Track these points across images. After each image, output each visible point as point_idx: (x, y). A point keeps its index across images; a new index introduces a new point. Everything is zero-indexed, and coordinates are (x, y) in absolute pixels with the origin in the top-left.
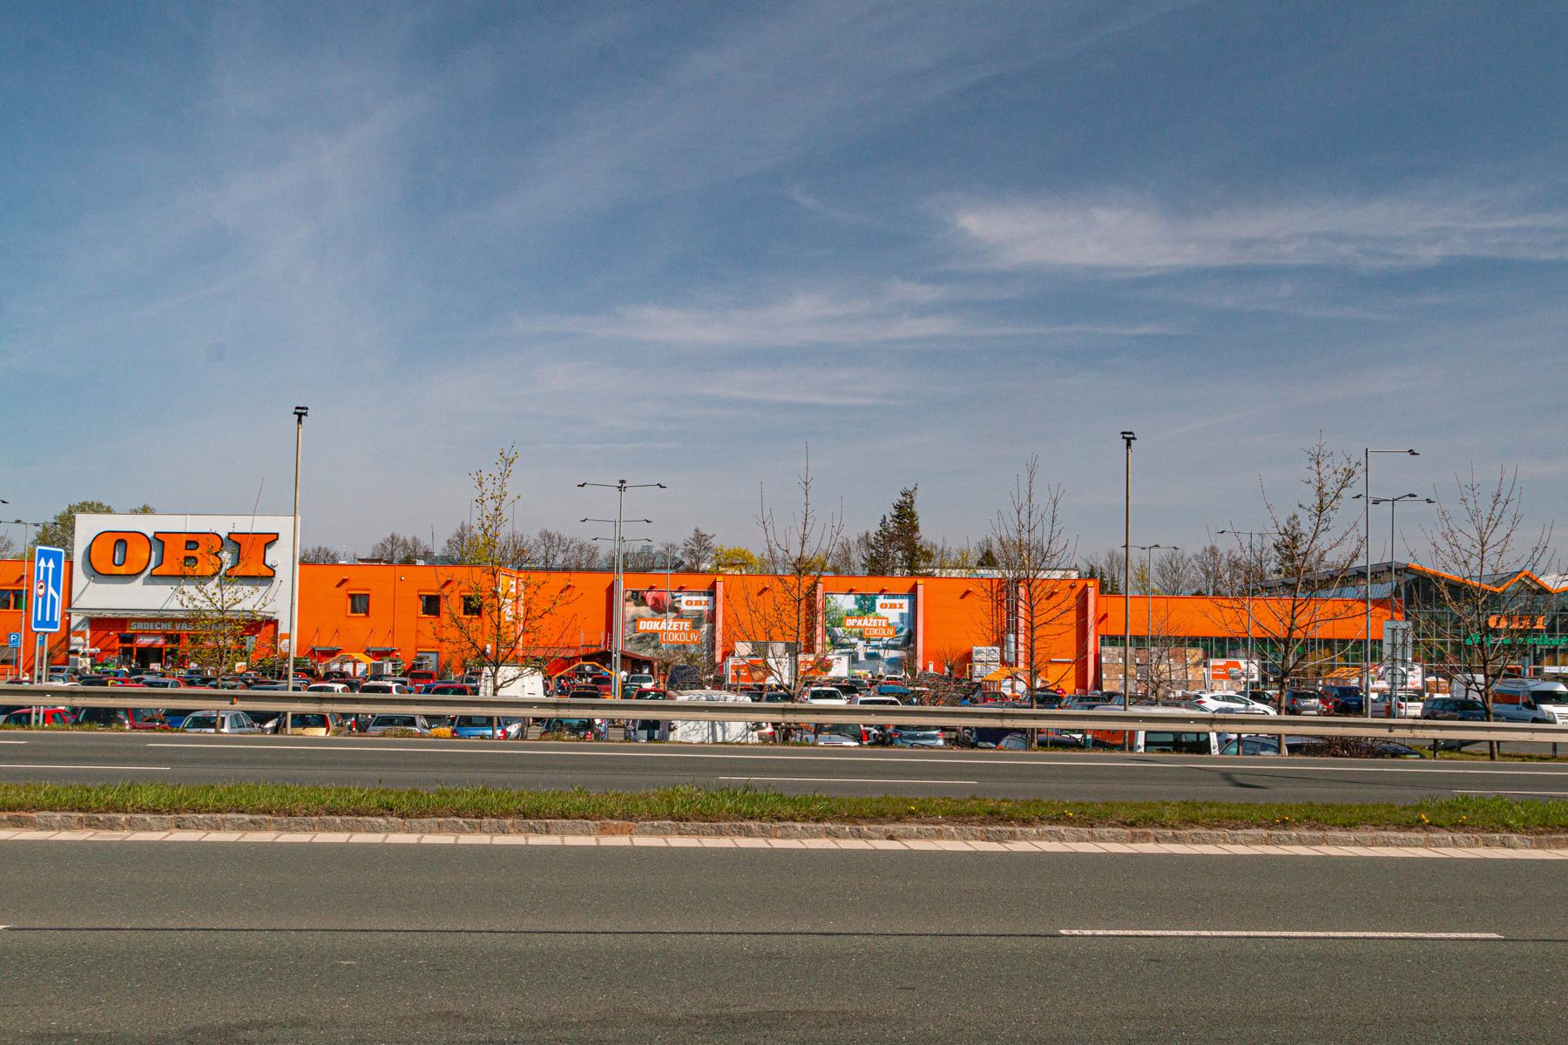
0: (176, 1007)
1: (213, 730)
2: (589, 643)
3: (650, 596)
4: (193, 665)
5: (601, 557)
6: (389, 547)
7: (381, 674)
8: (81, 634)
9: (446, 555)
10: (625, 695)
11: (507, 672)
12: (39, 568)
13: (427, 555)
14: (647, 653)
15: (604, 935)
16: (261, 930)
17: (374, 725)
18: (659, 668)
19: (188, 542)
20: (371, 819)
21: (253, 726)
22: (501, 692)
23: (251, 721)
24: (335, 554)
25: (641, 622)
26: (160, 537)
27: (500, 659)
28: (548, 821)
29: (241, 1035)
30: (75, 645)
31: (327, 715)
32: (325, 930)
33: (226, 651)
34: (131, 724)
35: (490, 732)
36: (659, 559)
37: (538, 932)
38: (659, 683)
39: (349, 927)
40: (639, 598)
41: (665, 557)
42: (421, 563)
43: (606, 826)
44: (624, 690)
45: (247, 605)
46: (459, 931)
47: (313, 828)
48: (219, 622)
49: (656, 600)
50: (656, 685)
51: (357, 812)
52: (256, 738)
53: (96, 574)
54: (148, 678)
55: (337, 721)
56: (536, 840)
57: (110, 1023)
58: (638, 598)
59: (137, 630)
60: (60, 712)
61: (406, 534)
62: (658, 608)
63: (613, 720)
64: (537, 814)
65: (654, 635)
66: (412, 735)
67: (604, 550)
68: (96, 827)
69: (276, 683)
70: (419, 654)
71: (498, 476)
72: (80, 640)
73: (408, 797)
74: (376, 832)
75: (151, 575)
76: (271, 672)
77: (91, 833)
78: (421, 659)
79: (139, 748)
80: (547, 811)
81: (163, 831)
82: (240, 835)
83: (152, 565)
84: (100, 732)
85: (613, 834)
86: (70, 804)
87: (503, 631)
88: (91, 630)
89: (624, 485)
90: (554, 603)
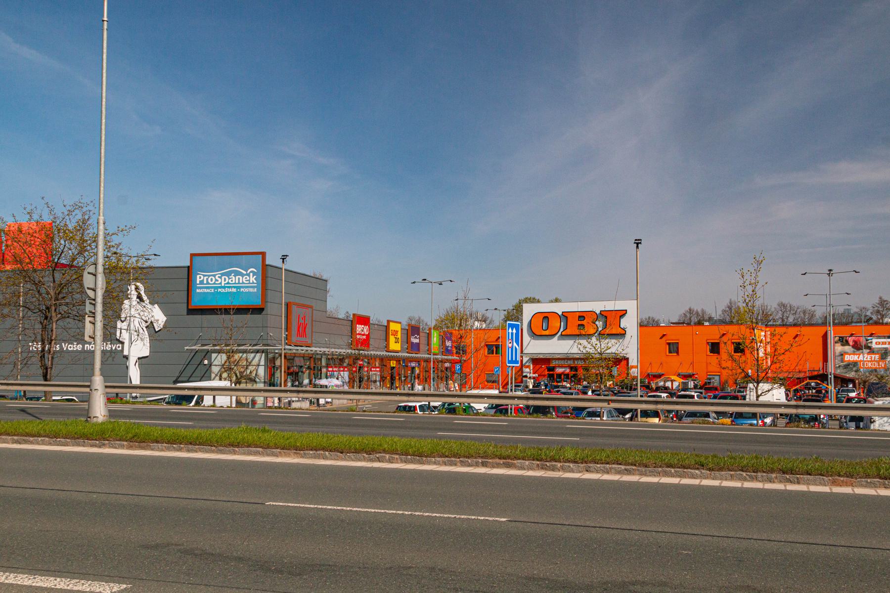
0: (596, 569)
1: (599, 419)
2: (812, 369)
3: (851, 340)
4: (585, 383)
5: (817, 317)
6: (688, 315)
7: (686, 387)
8: (528, 367)
9: (722, 318)
10: (838, 400)
11: (764, 386)
12: (509, 333)
13: (710, 319)
14: (851, 375)
15: (841, 548)
16: (637, 530)
17: (686, 417)
18: (860, 384)
19: (579, 317)
20: (693, 471)
21: (619, 417)
22: (761, 399)
23: (617, 414)
24: (658, 320)
25: (846, 356)
26: (565, 314)
27: (760, 379)
28: (798, 476)
29: (632, 588)
30: (525, 372)
31: (659, 411)
32: (672, 533)
33: (604, 375)
34: (556, 415)
35: (755, 422)
36: (856, 317)
37: (798, 543)
38: (860, 393)
39: (685, 532)
40: (844, 341)
41: (860, 315)
42: (707, 324)
43: (836, 481)
44: (837, 398)
45: (613, 350)
46: (750, 539)
47: (659, 474)
48: (600, 360)
49: (855, 342)
50: (858, 394)
51: (683, 467)
52: (621, 424)
53: (534, 335)
54: (563, 390)
55: (665, 414)
56: (791, 487)
57: (563, 575)
58: (843, 341)
59: (555, 364)
60: (521, 408)
61: (697, 308)
62: (857, 347)
63: (831, 416)
64: (791, 472)
65: (855, 363)
66: (709, 423)
67: (819, 313)
68: (546, 469)
69: (629, 393)
70: (708, 376)
71: (753, 271)
72: (527, 370)
73: (712, 459)
74: (695, 478)
75: (561, 335)
76: (627, 387)
77: (544, 473)
78: (710, 379)
79: (563, 428)
80: (797, 470)
81: (579, 473)
82: (620, 477)
83: (562, 330)
84: (541, 419)
85: (841, 486)
86: (532, 456)
87: (760, 362)
88: (533, 365)
89: (832, 272)
90: (792, 345)
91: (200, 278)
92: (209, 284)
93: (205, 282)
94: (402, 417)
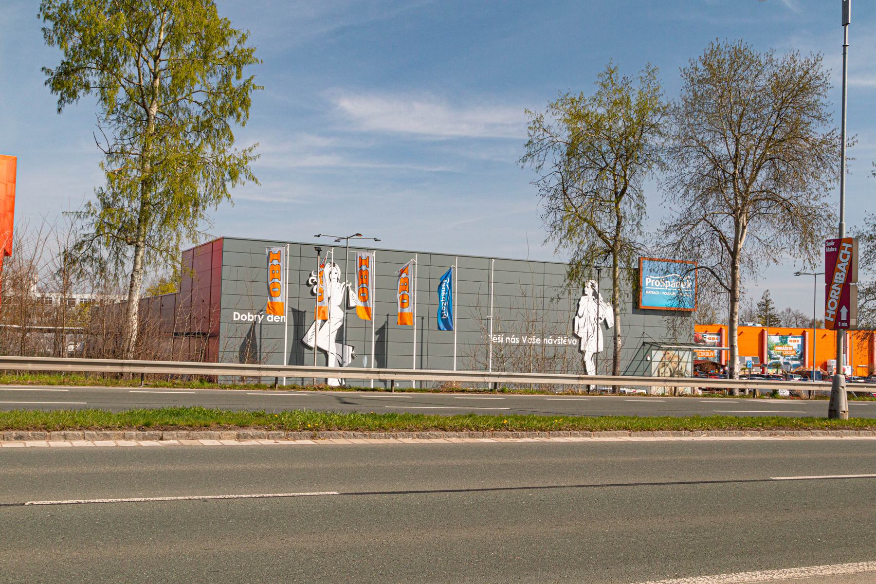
91: (649, 280)
92: (656, 287)
93: (652, 285)
94: (307, 393)
